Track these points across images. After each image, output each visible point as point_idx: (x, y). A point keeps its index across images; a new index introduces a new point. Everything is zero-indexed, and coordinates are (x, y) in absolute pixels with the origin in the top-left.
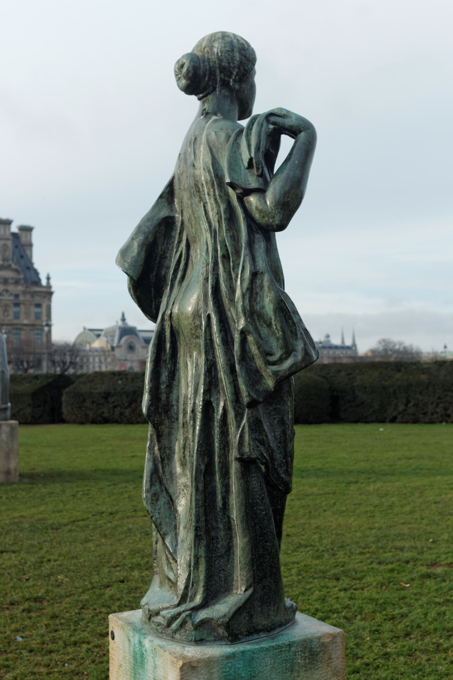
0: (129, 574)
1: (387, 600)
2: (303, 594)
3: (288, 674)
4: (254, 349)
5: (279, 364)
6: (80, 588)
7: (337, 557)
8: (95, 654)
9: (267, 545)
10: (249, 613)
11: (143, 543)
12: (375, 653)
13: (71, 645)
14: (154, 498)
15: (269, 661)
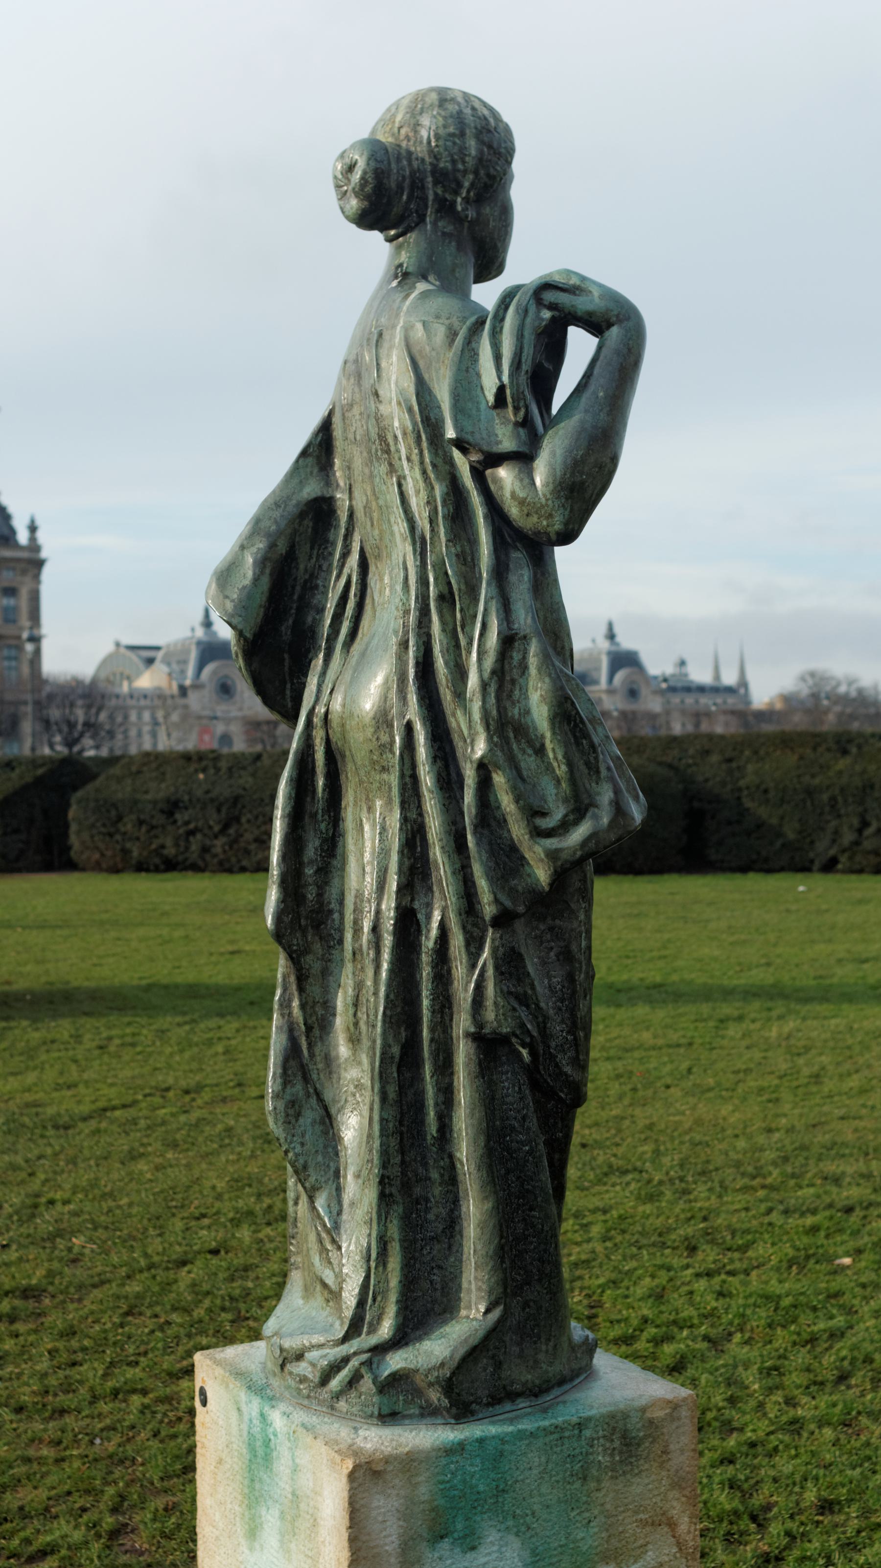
0: (229, 1235)
1: (801, 1298)
2: (614, 1282)
3: (577, 1485)
4: (506, 802)
5: (560, 835)
6: (121, 1266)
7: (692, 1197)
8: (159, 1416)
9: (533, 1217)
10: (493, 1357)
11: (260, 1163)
12: (770, 1420)
13: (105, 1397)
14: (291, 1112)
15: (537, 1459)
